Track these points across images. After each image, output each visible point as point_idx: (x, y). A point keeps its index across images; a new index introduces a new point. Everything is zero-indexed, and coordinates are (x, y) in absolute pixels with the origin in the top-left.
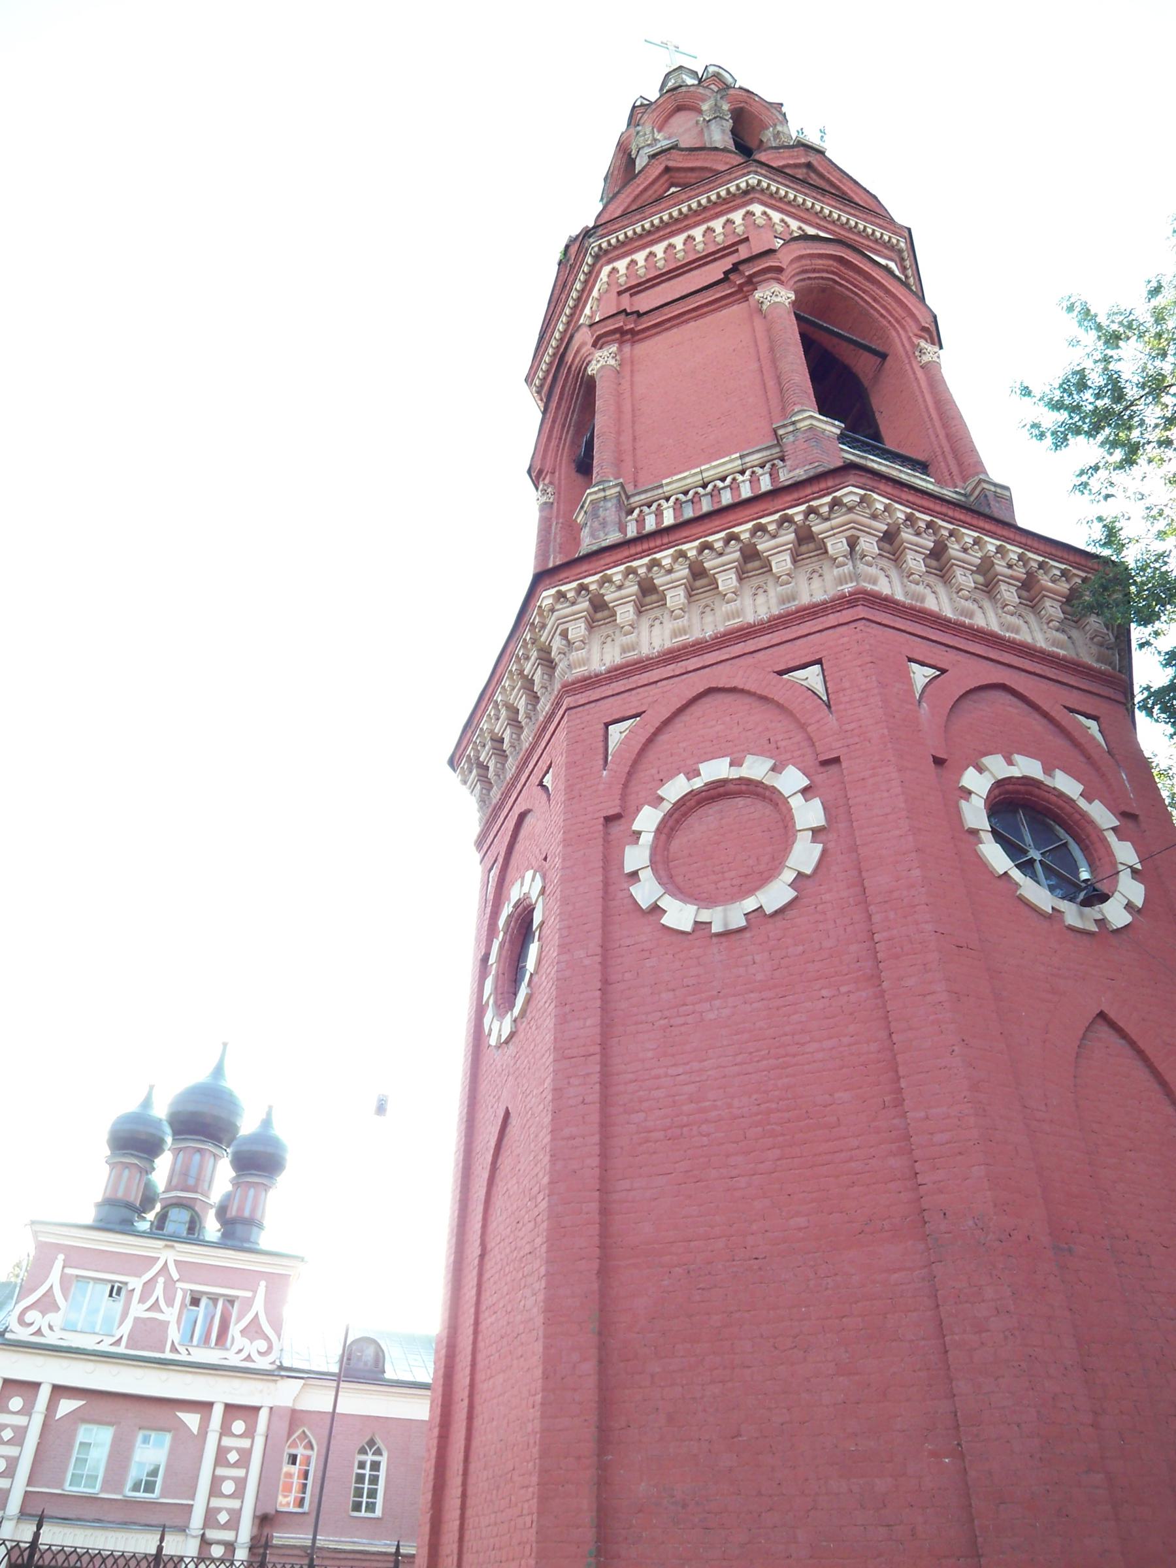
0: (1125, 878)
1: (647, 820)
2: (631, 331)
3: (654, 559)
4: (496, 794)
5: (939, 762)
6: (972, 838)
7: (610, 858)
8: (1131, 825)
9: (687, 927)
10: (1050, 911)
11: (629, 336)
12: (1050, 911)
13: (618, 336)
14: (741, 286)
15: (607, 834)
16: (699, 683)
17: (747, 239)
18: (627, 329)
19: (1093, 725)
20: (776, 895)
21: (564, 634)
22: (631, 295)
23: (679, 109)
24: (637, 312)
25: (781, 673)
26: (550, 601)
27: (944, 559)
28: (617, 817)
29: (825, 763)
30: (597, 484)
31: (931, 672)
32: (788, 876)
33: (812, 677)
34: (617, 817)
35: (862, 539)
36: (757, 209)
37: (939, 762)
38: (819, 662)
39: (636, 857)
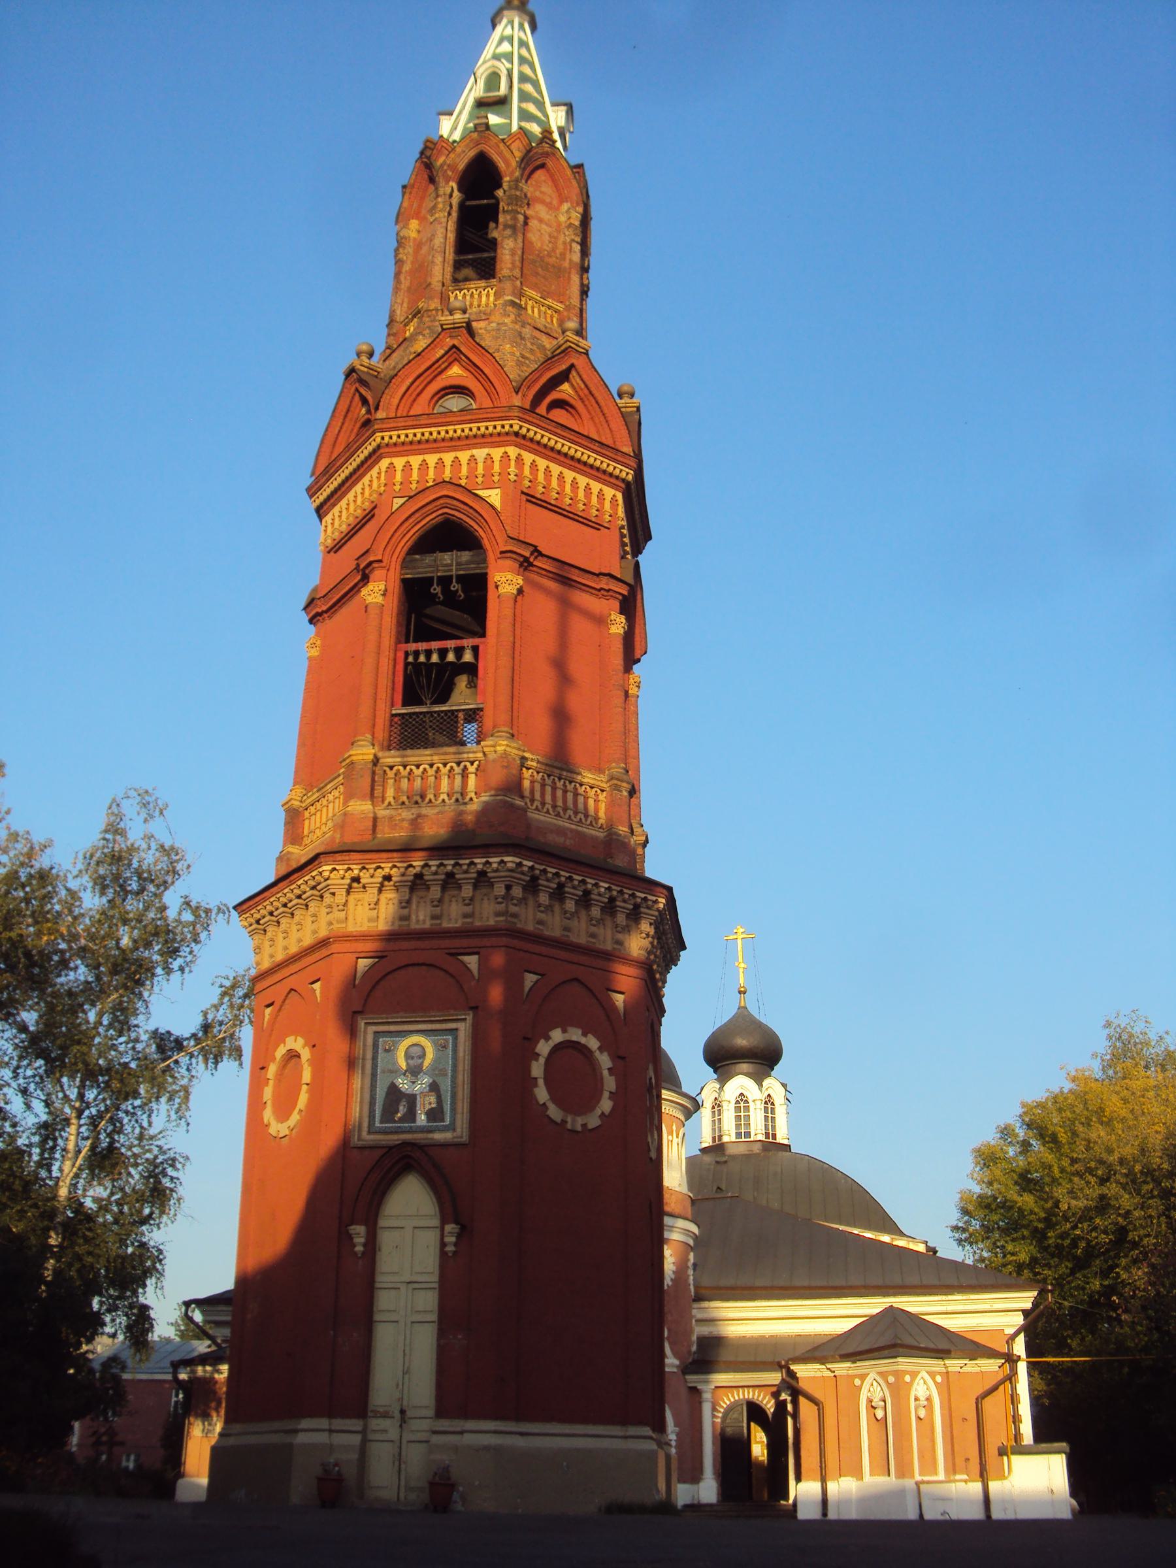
29: (619, 1057)
33: (472, 961)
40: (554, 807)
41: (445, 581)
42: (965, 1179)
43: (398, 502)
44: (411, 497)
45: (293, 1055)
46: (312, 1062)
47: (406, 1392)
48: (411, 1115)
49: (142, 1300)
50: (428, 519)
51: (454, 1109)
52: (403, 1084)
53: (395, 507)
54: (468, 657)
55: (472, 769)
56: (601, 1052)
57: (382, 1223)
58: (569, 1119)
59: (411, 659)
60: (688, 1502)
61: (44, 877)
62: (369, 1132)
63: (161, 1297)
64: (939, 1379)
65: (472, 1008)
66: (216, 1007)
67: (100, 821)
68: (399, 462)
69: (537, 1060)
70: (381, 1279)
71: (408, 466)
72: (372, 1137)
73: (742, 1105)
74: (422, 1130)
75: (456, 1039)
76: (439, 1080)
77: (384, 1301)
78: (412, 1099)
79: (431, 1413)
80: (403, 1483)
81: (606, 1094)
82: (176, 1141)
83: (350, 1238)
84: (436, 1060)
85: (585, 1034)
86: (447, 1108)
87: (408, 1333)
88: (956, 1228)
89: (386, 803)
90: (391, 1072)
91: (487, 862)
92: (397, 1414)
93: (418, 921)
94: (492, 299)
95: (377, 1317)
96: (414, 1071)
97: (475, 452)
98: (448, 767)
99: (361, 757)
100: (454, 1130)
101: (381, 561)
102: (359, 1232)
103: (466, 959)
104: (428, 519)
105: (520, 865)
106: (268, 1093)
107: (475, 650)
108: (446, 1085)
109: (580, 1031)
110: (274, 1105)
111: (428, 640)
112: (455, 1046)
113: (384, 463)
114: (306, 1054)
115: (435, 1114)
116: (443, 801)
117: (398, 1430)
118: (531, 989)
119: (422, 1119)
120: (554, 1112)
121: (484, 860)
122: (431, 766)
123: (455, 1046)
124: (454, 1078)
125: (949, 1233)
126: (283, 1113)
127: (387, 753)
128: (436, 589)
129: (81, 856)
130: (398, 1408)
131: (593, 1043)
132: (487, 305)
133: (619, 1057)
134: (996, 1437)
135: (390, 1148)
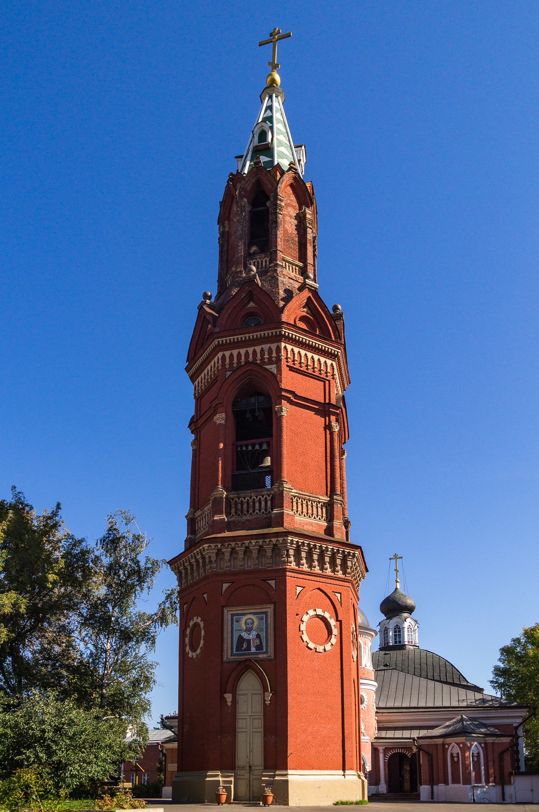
40: (307, 514)
41: (253, 411)
42: (495, 659)
43: (229, 373)
44: (234, 371)
45: (196, 625)
46: (204, 628)
47: (251, 759)
48: (249, 648)
49: (143, 721)
50: (243, 381)
51: (267, 645)
52: (245, 635)
53: (227, 376)
54: (265, 447)
55: (269, 498)
57: (238, 692)
59: (239, 449)
60: (374, 793)
61: (84, 553)
62: (231, 656)
63: (151, 719)
64: (483, 745)
65: (273, 603)
66: (164, 603)
67: (107, 526)
68: (227, 354)
70: (239, 716)
72: (232, 657)
73: (397, 630)
74: (253, 654)
75: (266, 616)
76: (260, 633)
77: (240, 724)
78: (249, 641)
79: (262, 768)
80: (251, 794)
82: (151, 658)
83: (225, 699)
84: (259, 625)
86: (264, 644)
87: (251, 736)
88: (492, 682)
89: (232, 515)
90: (239, 630)
91: (278, 540)
92: (248, 768)
93: (248, 566)
94: (268, 263)
95: (238, 730)
96: (249, 630)
97: (263, 346)
98: (258, 498)
99: (218, 495)
100: (267, 653)
101: (222, 403)
102: (228, 697)
103: (270, 582)
104: (243, 381)
106: (187, 640)
107: (268, 443)
108: (263, 635)
109: (321, 610)
110: (189, 645)
111: (246, 440)
112: (266, 618)
113: (220, 355)
114: (202, 625)
115: (259, 647)
116: (257, 513)
117: (249, 774)
119: (253, 649)
121: (276, 539)
122: (251, 498)
123: (266, 618)
124: (267, 631)
125: (489, 683)
126: (194, 650)
127: (230, 493)
128: (248, 415)
129: (99, 542)
130: (248, 765)
132: (266, 267)
134: (508, 768)
135: (241, 662)
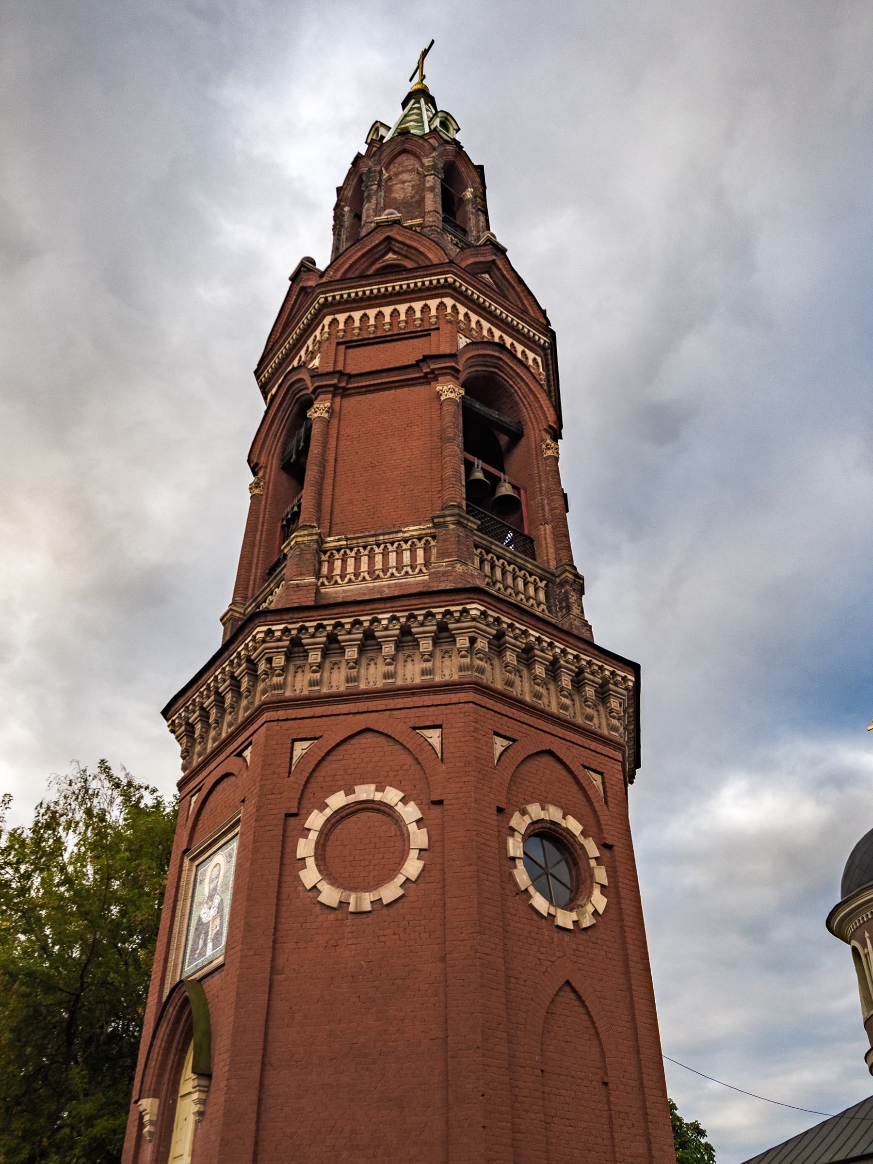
0: (597, 892)
1: (316, 820)
2: (344, 389)
3: (340, 622)
4: (196, 761)
5: (500, 810)
6: (510, 863)
7: (286, 846)
8: (607, 853)
9: (335, 904)
10: (546, 915)
11: (341, 391)
12: (546, 915)
13: (332, 389)
14: (426, 373)
15: (285, 826)
16: (360, 722)
17: (438, 329)
18: (342, 384)
19: (598, 778)
20: (390, 892)
21: (269, 661)
22: (347, 348)
23: (405, 151)
24: (349, 374)
25: (414, 728)
26: (262, 635)
27: (530, 655)
28: (295, 815)
29: (435, 803)
30: (305, 527)
31: (506, 743)
32: (400, 879)
33: (434, 737)
34: (295, 815)
35: (479, 640)
36: (449, 302)
37: (500, 810)
38: (439, 726)
39: (305, 848)
56: (405, 804)
58: (352, 900)
69: (306, 837)
71: (350, 319)
81: (414, 854)
85: (380, 789)
103: (427, 733)
105: (270, 632)
113: (327, 320)
118: (302, 757)
120: (330, 895)
131: (392, 796)
133: (435, 803)
